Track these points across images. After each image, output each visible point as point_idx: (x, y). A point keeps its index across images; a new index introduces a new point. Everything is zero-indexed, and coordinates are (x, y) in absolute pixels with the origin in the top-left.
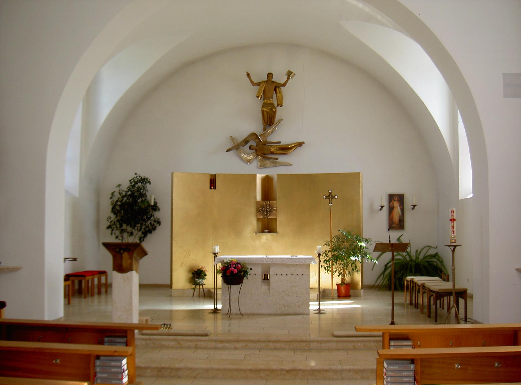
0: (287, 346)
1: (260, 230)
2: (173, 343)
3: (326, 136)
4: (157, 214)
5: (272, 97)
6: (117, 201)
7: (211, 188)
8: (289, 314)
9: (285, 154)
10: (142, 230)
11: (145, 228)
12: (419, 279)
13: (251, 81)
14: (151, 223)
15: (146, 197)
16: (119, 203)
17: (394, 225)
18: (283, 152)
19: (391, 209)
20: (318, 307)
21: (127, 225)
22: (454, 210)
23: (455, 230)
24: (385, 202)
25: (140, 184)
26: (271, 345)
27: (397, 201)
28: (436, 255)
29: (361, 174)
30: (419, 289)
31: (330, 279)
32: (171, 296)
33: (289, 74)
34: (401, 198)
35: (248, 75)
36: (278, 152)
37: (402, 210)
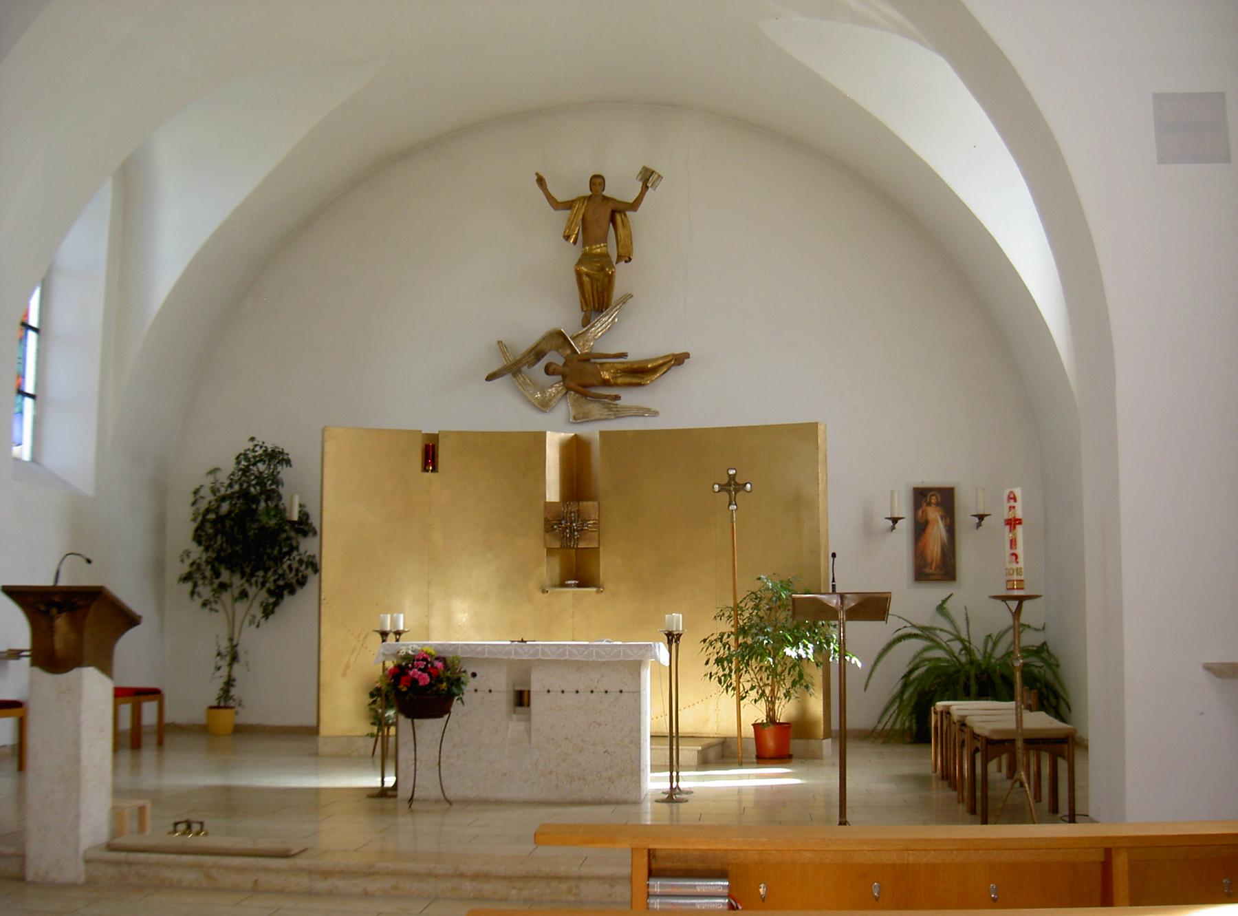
0: (514, 892)
1: (557, 582)
2: (190, 877)
3: (747, 334)
4: (307, 546)
5: (604, 239)
6: (208, 511)
7: (425, 470)
8: (607, 803)
9: (639, 385)
10: (268, 585)
11: (275, 581)
12: (959, 707)
13: (549, 197)
14: (290, 567)
15: (280, 497)
16: (212, 516)
17: (928, 570)
18: (635, 380)
19: (920, 528)
20: (667, 786)
21: (233, 572)
22: (1018, 492)
23: (1020, 550)
24: (904, 508)
25: (261, 467)
26: (468, 887)
27: (937, 504)
28: (1041, 650)
29: (821, 428)
30: (963, 741)
31: (718, 710)
32: (317, 754)
33: (648, 178)
34: (946, 498)
35: (541, 181)
36: (620, 380)
37: (951, 530)
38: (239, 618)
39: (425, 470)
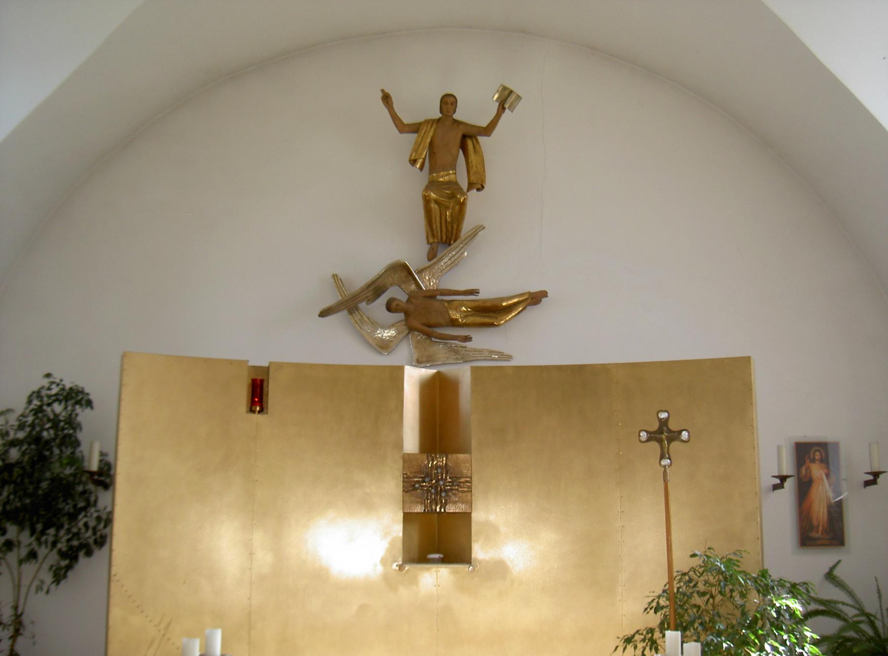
9: (492, 325)
10: (59, 545)
11: (69, 540)
17: (814, 534)
21: (22, 529)
25: (58, 408)
33: (506, 99)
35: (386, 98)
38: (25, 582)
39: (252, 411)
